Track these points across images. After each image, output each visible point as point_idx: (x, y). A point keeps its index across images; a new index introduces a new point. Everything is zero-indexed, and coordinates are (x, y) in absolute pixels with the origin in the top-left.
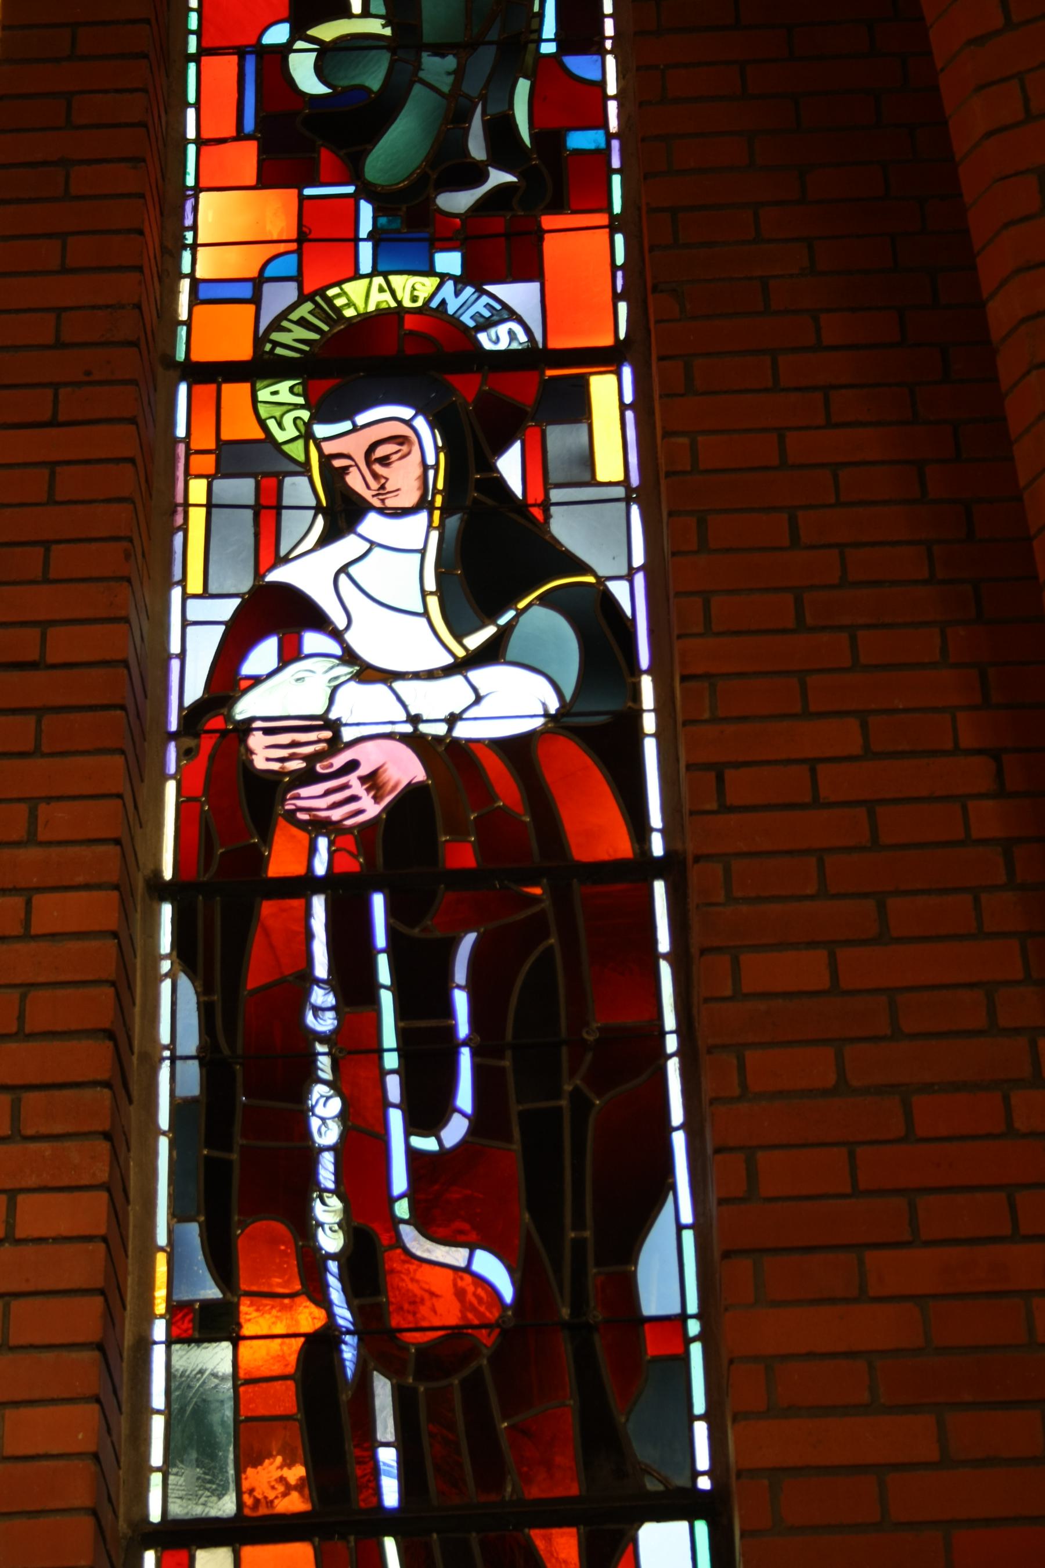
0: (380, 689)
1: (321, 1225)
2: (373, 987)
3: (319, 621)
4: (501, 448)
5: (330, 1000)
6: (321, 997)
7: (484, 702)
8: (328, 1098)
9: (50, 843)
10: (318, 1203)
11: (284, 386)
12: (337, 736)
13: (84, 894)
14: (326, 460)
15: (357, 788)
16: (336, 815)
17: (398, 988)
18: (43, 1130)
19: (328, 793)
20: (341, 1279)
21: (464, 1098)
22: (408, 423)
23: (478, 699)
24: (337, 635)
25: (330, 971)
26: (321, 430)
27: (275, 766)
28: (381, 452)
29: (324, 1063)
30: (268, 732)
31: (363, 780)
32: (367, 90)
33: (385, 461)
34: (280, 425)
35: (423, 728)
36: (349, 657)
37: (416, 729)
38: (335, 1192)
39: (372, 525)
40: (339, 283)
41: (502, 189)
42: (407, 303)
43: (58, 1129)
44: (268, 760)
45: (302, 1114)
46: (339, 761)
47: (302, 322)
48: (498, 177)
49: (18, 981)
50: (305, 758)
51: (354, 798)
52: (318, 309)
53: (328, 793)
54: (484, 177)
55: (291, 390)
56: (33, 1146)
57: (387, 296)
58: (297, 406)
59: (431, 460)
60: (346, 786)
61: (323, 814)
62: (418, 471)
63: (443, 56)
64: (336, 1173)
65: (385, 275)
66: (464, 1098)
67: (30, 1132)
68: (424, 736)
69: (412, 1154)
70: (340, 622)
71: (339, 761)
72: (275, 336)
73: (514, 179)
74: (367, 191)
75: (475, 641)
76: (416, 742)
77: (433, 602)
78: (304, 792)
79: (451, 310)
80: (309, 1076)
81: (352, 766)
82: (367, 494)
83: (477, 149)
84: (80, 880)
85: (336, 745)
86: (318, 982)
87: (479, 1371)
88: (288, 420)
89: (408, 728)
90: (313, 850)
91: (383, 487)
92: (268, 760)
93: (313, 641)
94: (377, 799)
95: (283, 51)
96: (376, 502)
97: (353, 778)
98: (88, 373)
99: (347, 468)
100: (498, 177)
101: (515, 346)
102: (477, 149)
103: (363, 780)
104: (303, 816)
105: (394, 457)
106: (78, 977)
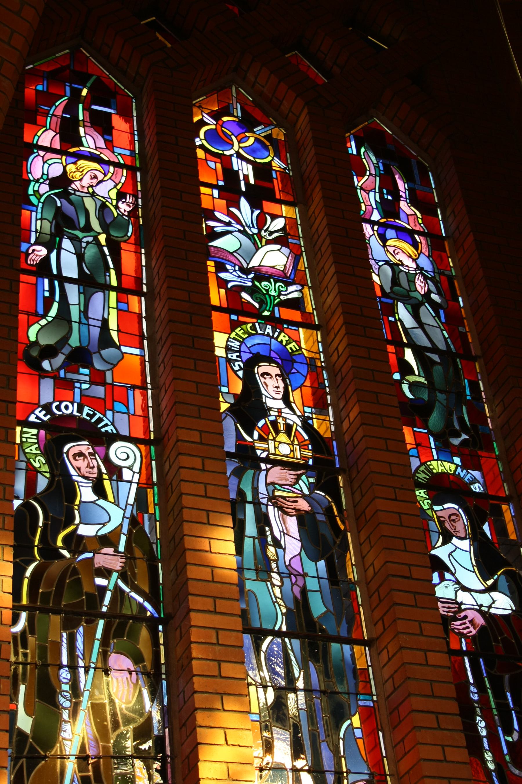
0: (467, 594)
1: (488, 760)
2: (485, 688)
3: (448, 570)
4: (483, 524)
5: (475, 690)
6: (473, 689)
7: (496, 602)
8: (481, 721)
9: (426, 636)
10: (485, 754)
11: (422, 491)
12: (460, 608)
13: (439, 654)
14: (439, 517)
15: (468, 624)
16: (465, 631)
17: (492, 688)
18: (446, 727)
19: (461, 624)
20: (497, 778)
21: (516, 726)
22: (457, 510)
23: (494, 602)
24: (453, 574)
25: (473, 681)
26: (436, 508)
27: (446, 613)
28: (453, 517)
29: (478, 710)
30: (442, 602)
31: (469, 621)
32: (424, 400)
33: (454, 521)
34: (424, 503)
35: (483, 608)
36: (457, 582)
37: (480, 608)
38: (489, 751)
39: (455, 540)
40: (430, 461)
41: (465, 440)
42: (449, 471)
43: (450, 728)
44: (443, 611)
45: (476, 725)
46: (462, 614)
47: (423, 471)
48: (464, 436)
49: (429, 679)
50: (453, 612)
51: (468, 628)
52: (426, 468)
53: (461, 624)
54: (460, 436)
55: (424, 492)
56: (445, 732)
57: (443, 468)
58: (427, 499)
59: (466, 523)
60: (465, 623)
61: (462, 631)
62: (463, 526)
63: (442, 394)
64: (488, 745)
65: (442, 461)
66: (516, 726)
67: (443, 727)
68: (482, 610)
69: (507, 742)
70: (454, 571)
71: (462, 614)
72: (417, 475)
73: (468, 437)
74: (430, 433)
75: (490, 582)
76: (480, 611)
77: (475, 568)
78: (455, 623)
79: (462, 476)
80: (475, 714)
81: (465, 617)
82: (452, 531)
83: (457, 426)
84: (437, 649)
85: (460, 610)
86: (471, 684)
87: (32, 747)
88: (425, 502)
89: (477, 608)
90: (461, 642)
91: (455, 529)
92: (443, 611)
93: (447, 575)
94: (474, 629)
95: (399, 383)
96: (455, 534)
97: (466, 621)
98: (402, 486)
99: (444, 521)
100: (464, 436)
101: (480, 491)
102: (457, 426)
103: (469, 621)
104: (457, 631)
105: (456, 520)
106: (444, 680)
